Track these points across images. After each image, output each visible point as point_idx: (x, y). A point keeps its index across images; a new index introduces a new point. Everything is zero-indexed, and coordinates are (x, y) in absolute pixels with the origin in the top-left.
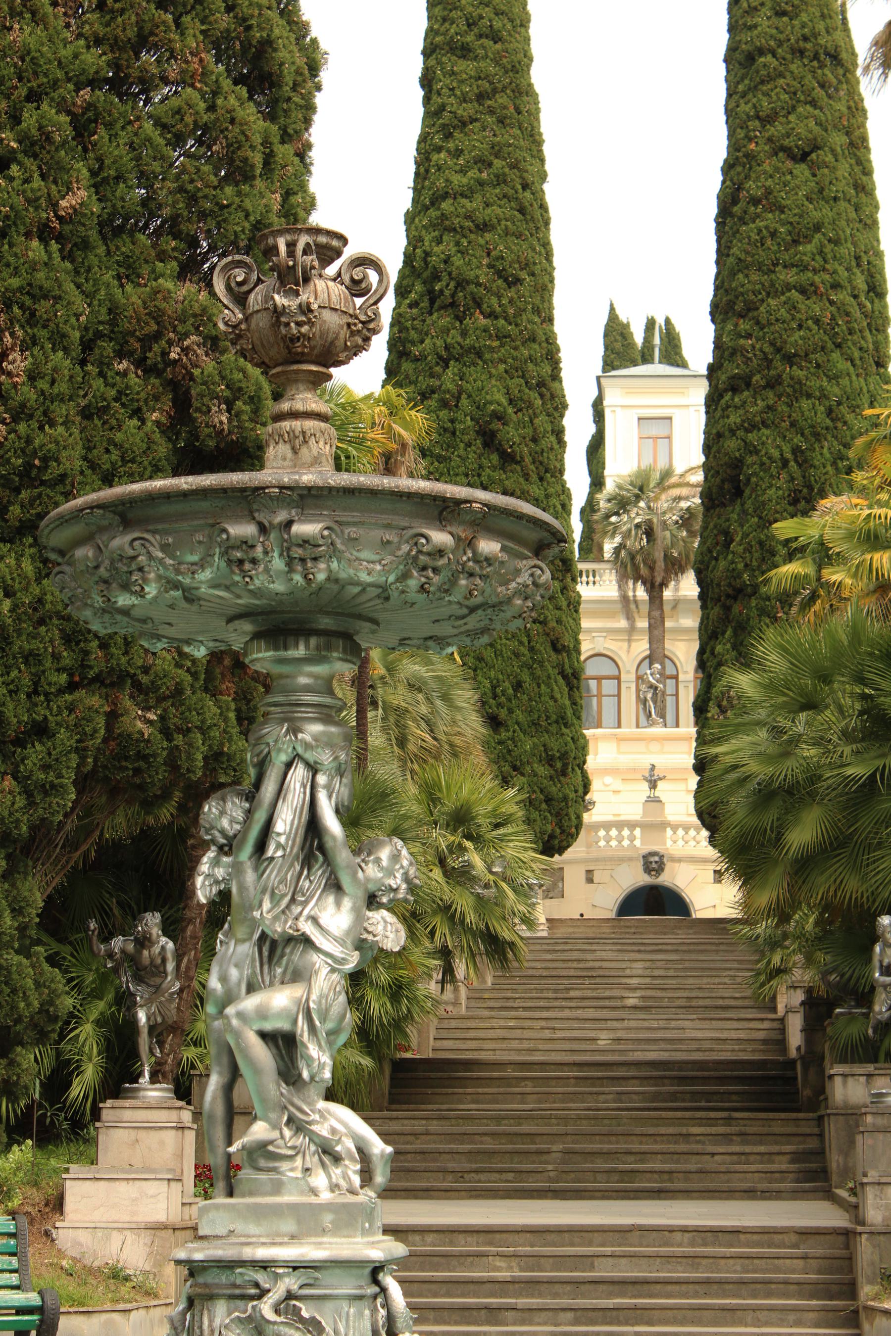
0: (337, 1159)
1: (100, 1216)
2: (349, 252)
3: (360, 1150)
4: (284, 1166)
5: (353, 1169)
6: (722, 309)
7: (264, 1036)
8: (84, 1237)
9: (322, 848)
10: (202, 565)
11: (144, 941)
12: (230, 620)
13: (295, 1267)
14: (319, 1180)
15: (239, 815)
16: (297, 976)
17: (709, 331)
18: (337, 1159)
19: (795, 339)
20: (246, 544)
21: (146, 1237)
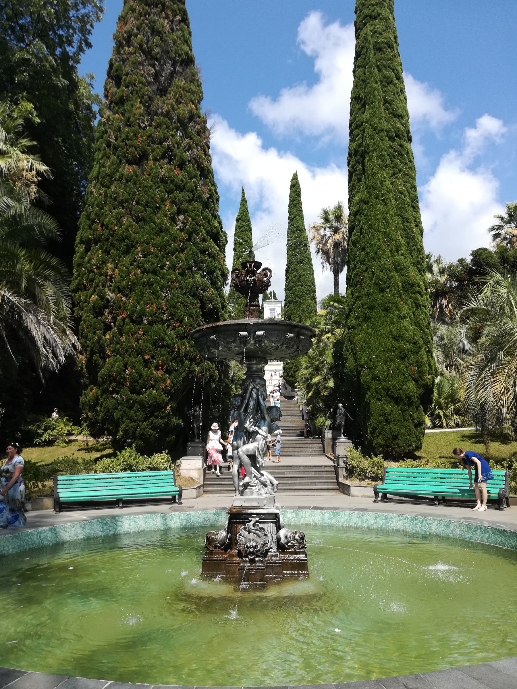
0: (266, 486)
1: (188, 467)
2: (262, 267)
3: (271, 483)
4: (253, 488)
5: (270, 487)
6: (287, 289)
7: (247, 455)
8: (185, 471)
9: (260, 409)
10: (233, 342)
11: (195, 411)
12: (237, 354)
13: (258, 515)
14: (263, 491)
15: (240, 401)
16: (254, 441)
17: (284, 294)
18: (266, 486)
19: (300, 294)
20: (245, 337)
21: (198, 471)
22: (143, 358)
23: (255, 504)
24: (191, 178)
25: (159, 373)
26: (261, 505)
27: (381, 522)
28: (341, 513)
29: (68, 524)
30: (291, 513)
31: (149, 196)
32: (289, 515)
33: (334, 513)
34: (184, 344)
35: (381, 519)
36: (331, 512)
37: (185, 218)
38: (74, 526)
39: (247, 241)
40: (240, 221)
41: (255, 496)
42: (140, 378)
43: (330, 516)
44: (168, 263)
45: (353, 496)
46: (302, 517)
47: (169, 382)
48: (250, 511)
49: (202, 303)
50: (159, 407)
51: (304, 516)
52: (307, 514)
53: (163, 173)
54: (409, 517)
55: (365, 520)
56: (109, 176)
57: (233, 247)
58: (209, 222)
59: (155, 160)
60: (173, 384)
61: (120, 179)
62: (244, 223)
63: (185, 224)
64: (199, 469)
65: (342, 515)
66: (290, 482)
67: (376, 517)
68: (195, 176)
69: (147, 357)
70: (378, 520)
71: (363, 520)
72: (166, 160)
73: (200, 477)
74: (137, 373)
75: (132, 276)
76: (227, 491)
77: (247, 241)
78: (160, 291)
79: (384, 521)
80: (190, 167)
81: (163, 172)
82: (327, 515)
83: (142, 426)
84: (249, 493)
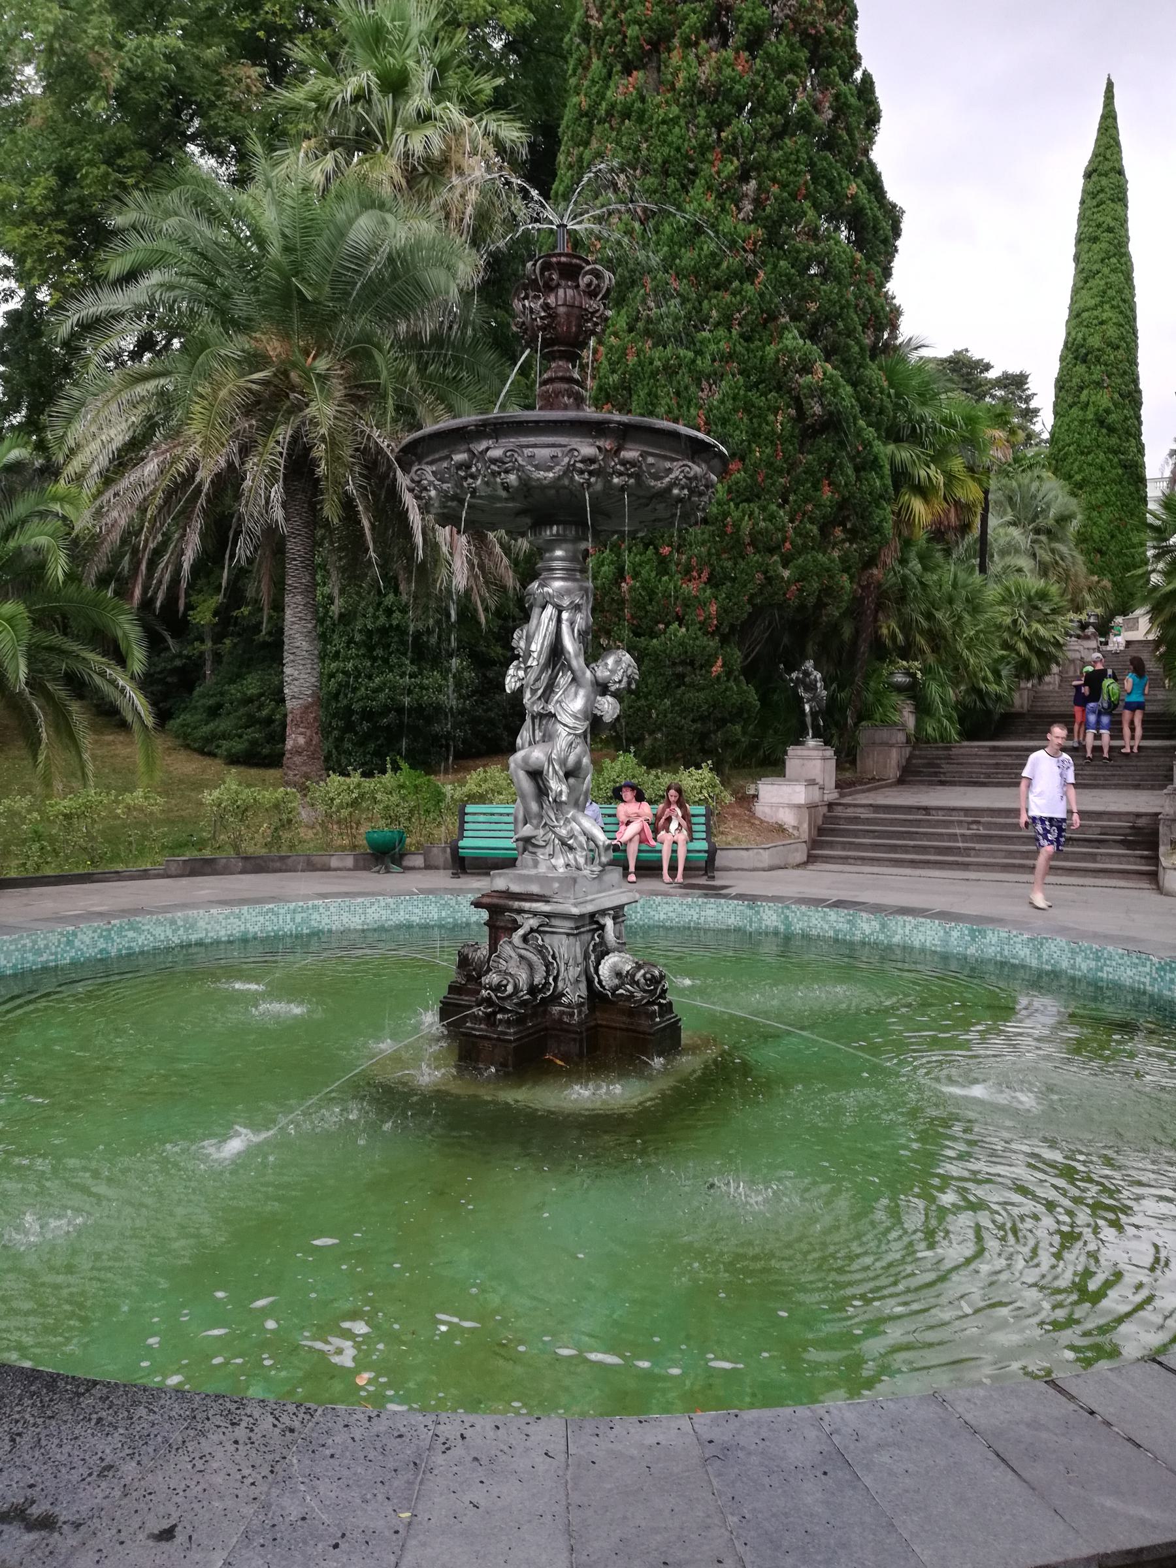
8: (767, 810)
22: (657, 552)
23: (535, 889)
24: (780, 75)
25: (691, 588)
26: (547, 892)
27: (1084, 966)
28: (990, 933)
29: (360, 900)
30: (868, 921)
31: (670, 145)
32: (865, 926)
33: (972, 931)
34: (751, 515)
35: (1086, 958)
36: (964, 927)
37: (760, 188)
38: (372, 904)
39: (1110, 230)
40: (1095, 178)
41: (542, 869)
42: (651, 600)
43: (962, 937)
44: (714, 313)
45: (1168, 894)
46: (895, 932)
47: (713, 609)
48: (516, 904)
49: (798, 403)
50: (694, 662)
51: (900, 931)
52: (908, 927)
53: (703, 77)
54: (1155, 960)
55: (1045, 957)
56: (586, 115)
57: (1073, 250)
58: (830, 185)
59: (688, 44)
60: (724, 611)
61: (609, 114)
62: (1104, 181)
63: (758, 203)
64: (799, 806)
65: (992, 937)
66: (1024, 848)
67: (1072, 951)
68: (793, 67)
69: (666, 550)
70: (1079, 960)
71: (1040, 956)
72: (714, 41)
73: (800, 823)
74: (644, 588)
75: (632, 360)
76: (985, 865)
77: (1110, 230)
78: (693, 389)
79: (1093, 964)
80: (777, 45)
81: (705, 73)
82: (955, 934)
83: (662, 708)
84: (530, 863)
